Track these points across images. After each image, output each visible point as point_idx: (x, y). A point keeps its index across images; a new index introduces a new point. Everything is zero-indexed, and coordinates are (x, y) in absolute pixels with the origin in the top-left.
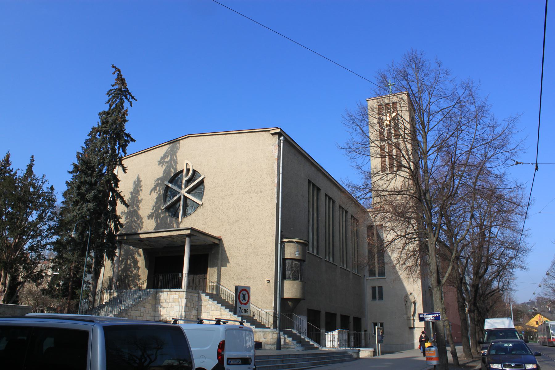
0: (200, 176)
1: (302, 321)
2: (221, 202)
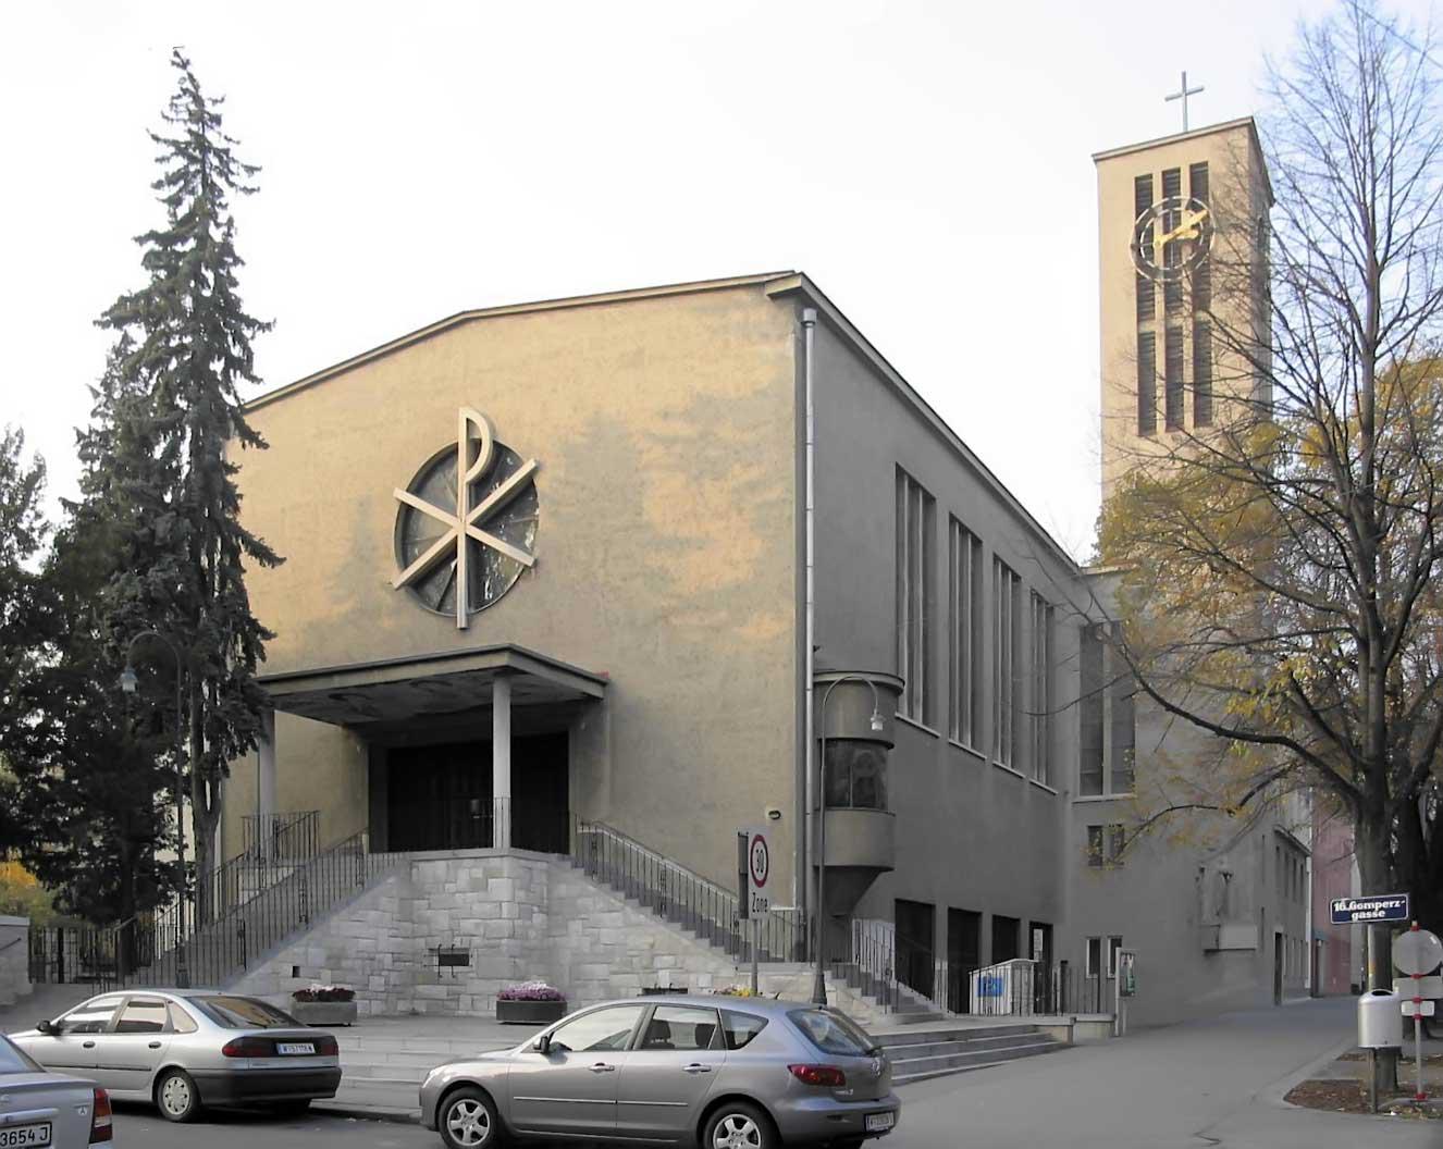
0: (517, 467)
1: (877, 940)
2: (600, 556)
